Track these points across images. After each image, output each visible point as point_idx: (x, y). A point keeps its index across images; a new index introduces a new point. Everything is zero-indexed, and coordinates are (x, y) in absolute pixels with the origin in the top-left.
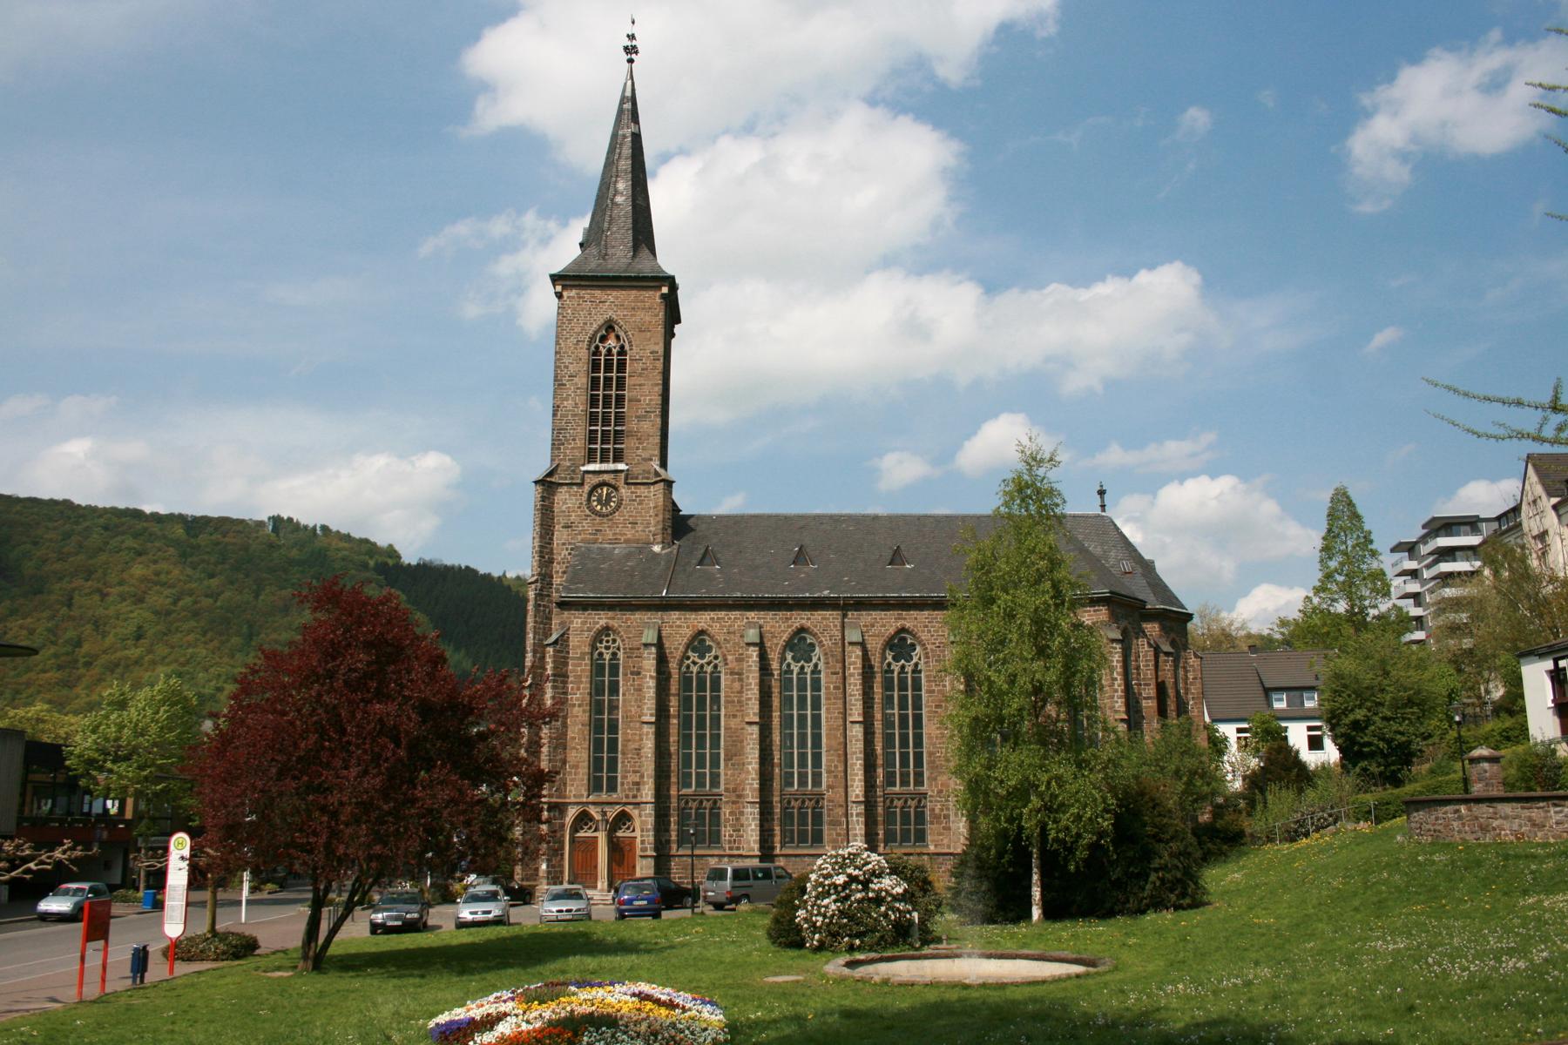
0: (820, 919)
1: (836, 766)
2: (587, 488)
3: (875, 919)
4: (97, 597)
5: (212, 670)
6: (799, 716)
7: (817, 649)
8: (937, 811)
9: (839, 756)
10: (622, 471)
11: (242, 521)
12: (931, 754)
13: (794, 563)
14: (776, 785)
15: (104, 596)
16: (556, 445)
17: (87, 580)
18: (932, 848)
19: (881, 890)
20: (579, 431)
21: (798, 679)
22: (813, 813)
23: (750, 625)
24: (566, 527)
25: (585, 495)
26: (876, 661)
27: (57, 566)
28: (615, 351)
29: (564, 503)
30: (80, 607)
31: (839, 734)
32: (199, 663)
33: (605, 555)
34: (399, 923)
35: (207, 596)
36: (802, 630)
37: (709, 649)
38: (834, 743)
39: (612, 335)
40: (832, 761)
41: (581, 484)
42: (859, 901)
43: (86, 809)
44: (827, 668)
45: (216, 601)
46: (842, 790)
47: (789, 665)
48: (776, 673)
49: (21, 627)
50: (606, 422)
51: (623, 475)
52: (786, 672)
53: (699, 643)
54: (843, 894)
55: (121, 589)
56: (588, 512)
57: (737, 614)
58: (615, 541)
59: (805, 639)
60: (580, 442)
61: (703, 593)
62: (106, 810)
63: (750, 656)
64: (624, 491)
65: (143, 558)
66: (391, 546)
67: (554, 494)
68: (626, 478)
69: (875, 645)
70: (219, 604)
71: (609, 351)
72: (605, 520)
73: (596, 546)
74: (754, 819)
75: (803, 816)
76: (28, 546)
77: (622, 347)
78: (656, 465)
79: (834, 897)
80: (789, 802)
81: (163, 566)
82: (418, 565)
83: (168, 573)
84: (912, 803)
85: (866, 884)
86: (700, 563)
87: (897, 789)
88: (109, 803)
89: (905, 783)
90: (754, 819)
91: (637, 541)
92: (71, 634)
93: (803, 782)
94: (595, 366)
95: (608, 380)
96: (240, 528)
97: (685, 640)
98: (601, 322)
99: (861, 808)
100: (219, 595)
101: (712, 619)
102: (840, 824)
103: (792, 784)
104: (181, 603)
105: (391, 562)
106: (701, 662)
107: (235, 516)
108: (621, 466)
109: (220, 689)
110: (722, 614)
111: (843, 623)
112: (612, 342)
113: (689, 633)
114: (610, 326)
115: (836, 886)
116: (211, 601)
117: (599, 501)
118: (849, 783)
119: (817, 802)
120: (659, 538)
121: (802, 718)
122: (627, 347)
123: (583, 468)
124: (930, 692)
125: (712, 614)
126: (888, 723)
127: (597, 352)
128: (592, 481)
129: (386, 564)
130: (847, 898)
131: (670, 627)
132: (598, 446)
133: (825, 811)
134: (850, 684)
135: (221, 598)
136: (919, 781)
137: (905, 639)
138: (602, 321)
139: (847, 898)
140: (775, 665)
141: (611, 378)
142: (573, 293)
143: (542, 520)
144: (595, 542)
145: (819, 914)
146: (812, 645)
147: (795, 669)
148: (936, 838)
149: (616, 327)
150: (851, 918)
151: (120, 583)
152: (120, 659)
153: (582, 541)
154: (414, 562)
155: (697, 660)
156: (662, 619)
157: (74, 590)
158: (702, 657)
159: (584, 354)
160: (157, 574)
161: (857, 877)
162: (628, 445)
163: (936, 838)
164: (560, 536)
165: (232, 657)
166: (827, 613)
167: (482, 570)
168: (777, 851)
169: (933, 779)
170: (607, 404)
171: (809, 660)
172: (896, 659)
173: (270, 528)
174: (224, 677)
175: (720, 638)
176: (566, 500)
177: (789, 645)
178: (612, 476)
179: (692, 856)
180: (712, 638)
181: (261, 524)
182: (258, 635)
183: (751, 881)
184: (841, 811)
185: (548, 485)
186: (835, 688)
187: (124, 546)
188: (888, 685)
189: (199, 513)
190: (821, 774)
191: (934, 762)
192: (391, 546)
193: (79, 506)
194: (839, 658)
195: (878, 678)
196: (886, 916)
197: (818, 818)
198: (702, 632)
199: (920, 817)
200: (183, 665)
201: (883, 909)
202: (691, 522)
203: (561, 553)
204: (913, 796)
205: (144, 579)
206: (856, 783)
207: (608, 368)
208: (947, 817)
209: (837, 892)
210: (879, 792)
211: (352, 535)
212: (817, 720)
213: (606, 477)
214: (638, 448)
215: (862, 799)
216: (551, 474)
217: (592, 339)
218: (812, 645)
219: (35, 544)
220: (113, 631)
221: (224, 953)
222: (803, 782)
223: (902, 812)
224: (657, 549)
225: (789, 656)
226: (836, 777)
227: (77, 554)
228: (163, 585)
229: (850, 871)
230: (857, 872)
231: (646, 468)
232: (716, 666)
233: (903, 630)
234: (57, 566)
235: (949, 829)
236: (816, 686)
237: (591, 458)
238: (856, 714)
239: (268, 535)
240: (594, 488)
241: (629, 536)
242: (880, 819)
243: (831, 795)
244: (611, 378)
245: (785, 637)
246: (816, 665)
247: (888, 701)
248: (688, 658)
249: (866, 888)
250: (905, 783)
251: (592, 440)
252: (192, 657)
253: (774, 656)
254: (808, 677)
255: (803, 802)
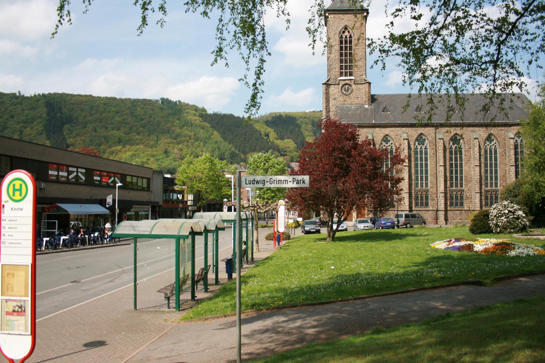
0: (501, 223)
1: (433, 181)
2: (341, 86)
3: (517, 224)
4: (104, 129)
5: (146, 153)
6: (457, 161)
7: (426, 141)
8: (468, 196)
9: (434, 177)
10: (353, 79)
11: (151, 100)
12: (465, 177)
13: (416, 111)
14: (413, 187)
15: (106, 128)
16: (329, 71)
17: (100, 123)
18: (466, 208)
19: (519, 215)
20: (337, 65)
21: (420, 151)
22: (425, 196)
23: (404, 132)
24: (334, 99)
25: (340, 88)
26: (447, 145)
27: (90, 118)
28: (348, 37)
29: (333, 91)
30: (99, 132)
31: (434, 169)
32: (141, 151)
33: (349, 109)
34: (315, 230)
35: (141, 127)
36: (421, 134)
37: (389, 141)
38: (433, 173)
39: (347, 31)
40: (432, 179)
41: (339, 84)
42: (512, 218)
43: (171, 198)
44: (430, 147)
45: (144, 129)
46: (435, 189)
47: (417, 146)
48: (413, 149)
49: (81, 140)
50: (346, 62)
51: (353, 81)
52: (416, 149)
53: (420, 138)
54: (507, 216)
55: (112, 125)
56: (341, 94)
57: (399, 129)
58: (351, 104)
59: (422, 137)
60: (338, 69)
61: (387, 122)
62: (178, 198)
63: (405, 143)
64: (354, 86)
65: (119, 114)
66: (203, 107)
67: (329, 88)
68: (354, 82)
69: (447, 139)
70: (145, 130)
71: (346, 37)
72: (347, 96)
73: (345, 106)
74: (407, 198)
75: (422, 197)
76: (80, 112)
77: (351, 35)
78: (364, 77)
79: (504, 217)
80: (417, 193)
81: (125, 117)
82: (214, 114)
83: (127, 119)
84: (459, 193)
85: (514, 213)
86: (383, 111)
87: (454, 188)
88: (179, 195)
89: (457, 186)
90: (407, 198)
91: (359, 104)
92: (97, 142)
93: (422, 186)
94: (341, 42)
95: (346, 47)
96: (150, 102)
97: (381, 138)
98: (343, 26)
99: (443, 195)
100: (145, 126)
101: (390, 131)
102: (434, 200)
103: (418, 187)
104: (133, 130)
105: (204, 113)
106: (387, 145)
107: (148, 98)
108: (352, 78)
109: (148, 160)
110: (394, 129)
111: (436, 132)
112: (346, 33)
113: (382, 135)
114: (346, 28)
115: (505, 213)
116: (142, 129)
117: (345, 90)
118: (438, 186)
119: (427, 193)
120: (367, 103)
121: (421, 164)
122: (352, 35)
123: (339, 79)
124: (466, 155)
125: (390, 129)
126: (451, 165)
127: (341, 37)
128: (342, 83)
129: (202, 114)
130: (508, 217)
131: (376, 133)
132: (348, 71)
133: (429, 196)
134: (439, 153)
135: (146, 128)
136: (461, 186)
137: (457, 137)
138: (343, 26)
139: (508, 217)
140: (412, 146)
141: (347, 46)
142: (332, 16)
143: (326, 97)
144: (344, 104)
145: (500, 222)
146: (425, 139)
147: (419, 147)
148: (467, 205)
149: (348, 28)
150: (510, 223)
151: (112, 123)
152: (114, 150)
153: (340, 104)
154: (212, 113)
155: (385, 145)
156: (373, 131)
157: (97, 126)
158: (387, 143)
159: (337, 38)
160: (124, 120)
161: (511, 211)
162: (355, 70)
163: (467, 205)
164: (332, 102)
165: (152, 148)
166: (430, 128)
167: (236, 115)
168: (414, 209)
169: (466, 185)
170: (346, 56)
171: (423, 144)
172: (453, 144)
173: (161, 102)
174: (150, 155)
175: (393, 137)
176: (334, 90)
177: (417, 140)
178: (349, 81)
179: (397, 210)
180: (390, 137)
181: (157, 101)
182: (160, 140)
183: (410, 218)
184: (435, 196)
185: (327, 85)
186: (433, 154)
187: (111, 110)
188: (451, 153)
189: (135, 98)
190: (428, 183)
191: (467, 179)
192: (203, 107)
193: (95, 97)
194: (434, 144)
195: (448, 151)
196: (520, 223)
197: (427, 198)
198: (387, 135)
199: (462, 197)
200: (136, 151)
201: (520, 221)
202: (375, 97)
203: (332, 109)
204: (459, 191)
205: (119, 122)
206: (441, 186)
207: (346, 43)
208: (471, 198)
209: (506, 216)
210: (448, 189)
211: (189, 103)
212: (426, 165)
213: (347, 82)
214: (358, 71)
215: (443, 191)
216: (328, 81)
217: (340, 33)
218: (425, 139)
219: (82, 110)
220: (111, 140)
221: (285, 238)
222: (422, 186)
223: (455, 196)
224: (366, 106)
225: (417, 143)
226: (433, 184)
227: (96, 113)
228: (126, 123)
229: (509, 209)
230: (511, 209)
231: (361, 78)
232: (392, 147)
233: (456, 134)
234: (90, 118)
235: (472, 202)
236: (426, 154)
237: (341, 74)
238: (441, 163)
239: (160, 105)
240: (343, 86)
241: (356, 102)
242: (448, 198)
243: (432, 191)
244: (347, 46)
245: (416, 136)
246: (426, 146)
247: (451, 159)
248: (382, 144)
249: (514, 214)
250: (457, 186)
251: (341, 69)
252: (138, 149)
253: (412, 143)
254: (423, 150)
255: (422, 193)
